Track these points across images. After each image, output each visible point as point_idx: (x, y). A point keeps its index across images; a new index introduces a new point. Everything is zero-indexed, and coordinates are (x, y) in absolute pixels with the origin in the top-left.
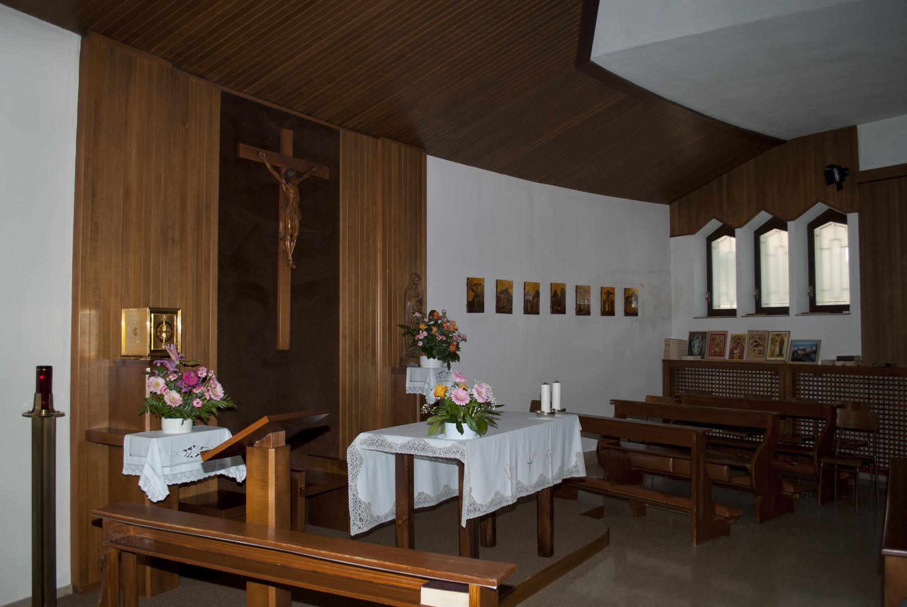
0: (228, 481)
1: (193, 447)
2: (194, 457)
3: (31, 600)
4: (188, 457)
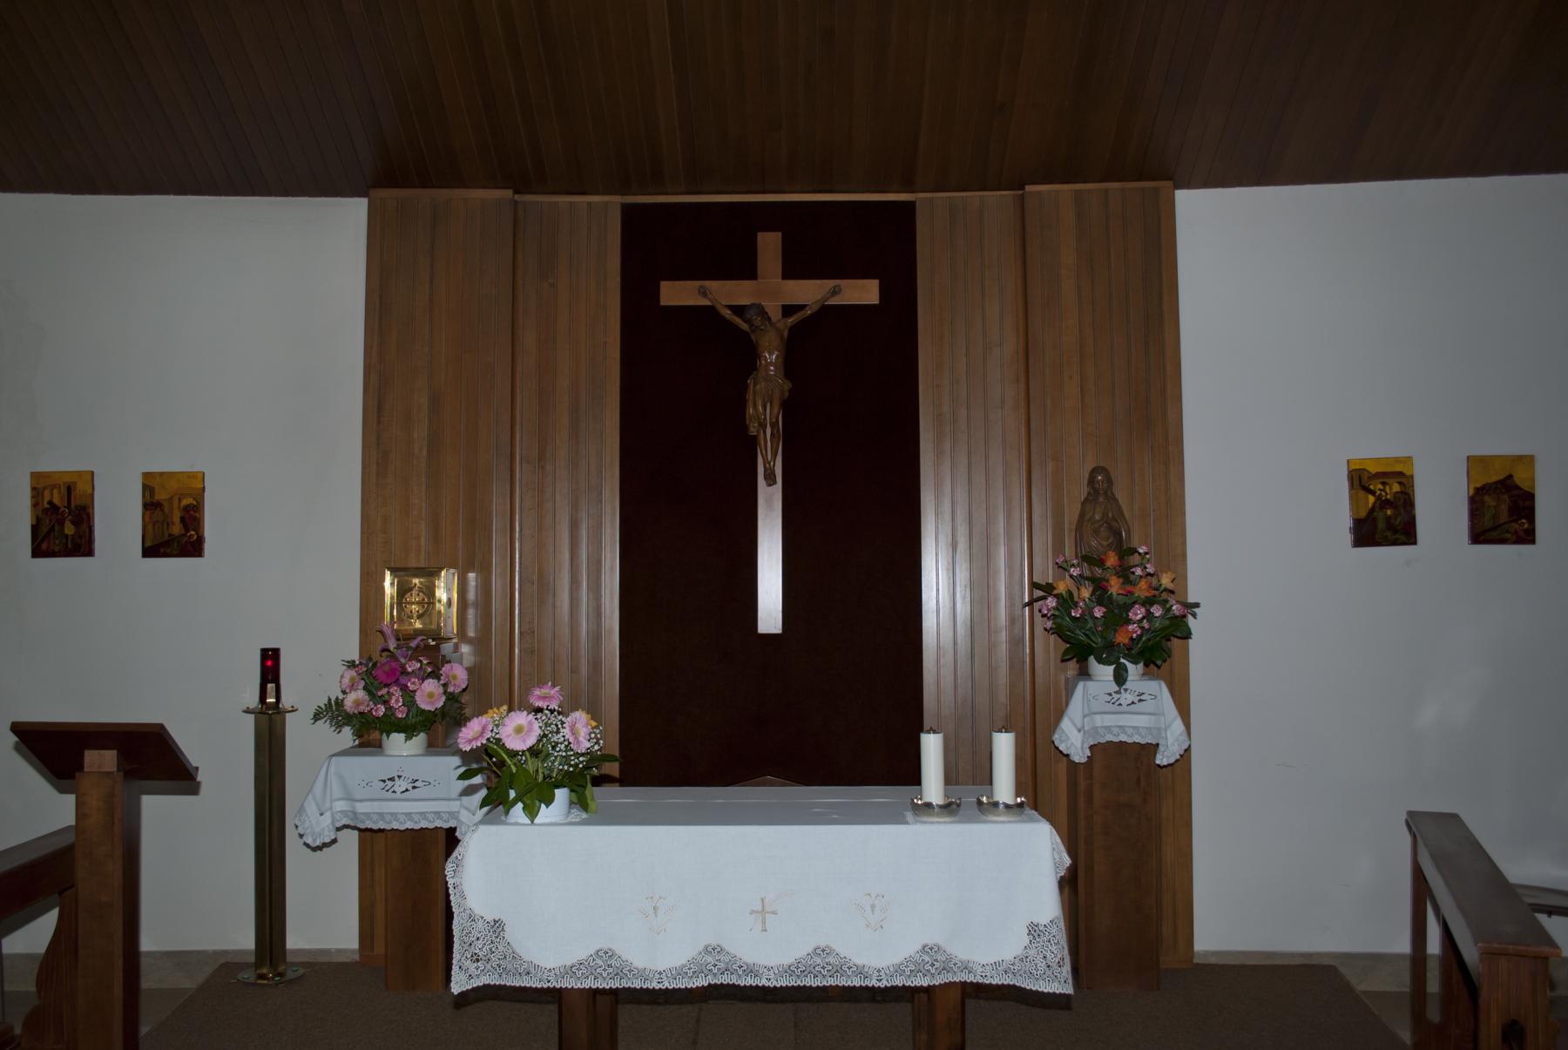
0: (1061, 755)
1: (396, 778)
2: (398, 793)
3: (36, 966)
4: (387, 791)
